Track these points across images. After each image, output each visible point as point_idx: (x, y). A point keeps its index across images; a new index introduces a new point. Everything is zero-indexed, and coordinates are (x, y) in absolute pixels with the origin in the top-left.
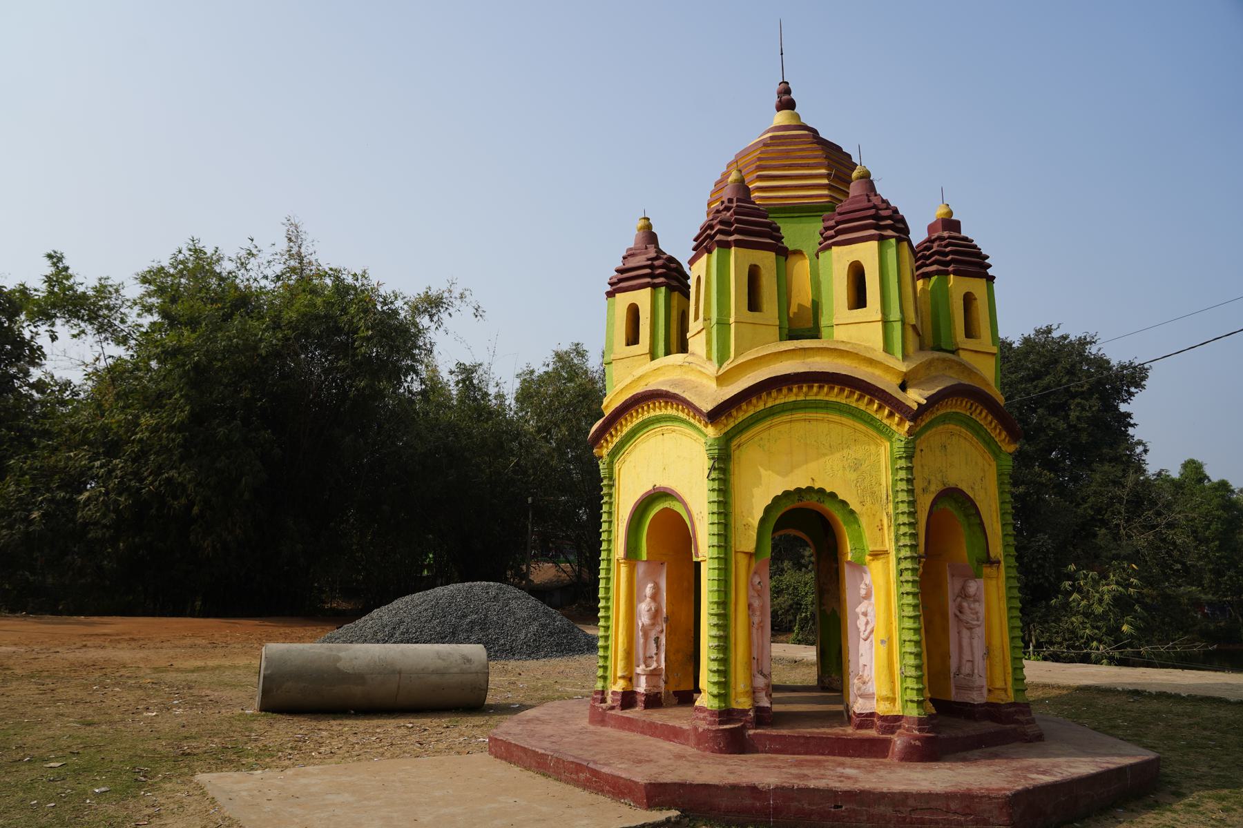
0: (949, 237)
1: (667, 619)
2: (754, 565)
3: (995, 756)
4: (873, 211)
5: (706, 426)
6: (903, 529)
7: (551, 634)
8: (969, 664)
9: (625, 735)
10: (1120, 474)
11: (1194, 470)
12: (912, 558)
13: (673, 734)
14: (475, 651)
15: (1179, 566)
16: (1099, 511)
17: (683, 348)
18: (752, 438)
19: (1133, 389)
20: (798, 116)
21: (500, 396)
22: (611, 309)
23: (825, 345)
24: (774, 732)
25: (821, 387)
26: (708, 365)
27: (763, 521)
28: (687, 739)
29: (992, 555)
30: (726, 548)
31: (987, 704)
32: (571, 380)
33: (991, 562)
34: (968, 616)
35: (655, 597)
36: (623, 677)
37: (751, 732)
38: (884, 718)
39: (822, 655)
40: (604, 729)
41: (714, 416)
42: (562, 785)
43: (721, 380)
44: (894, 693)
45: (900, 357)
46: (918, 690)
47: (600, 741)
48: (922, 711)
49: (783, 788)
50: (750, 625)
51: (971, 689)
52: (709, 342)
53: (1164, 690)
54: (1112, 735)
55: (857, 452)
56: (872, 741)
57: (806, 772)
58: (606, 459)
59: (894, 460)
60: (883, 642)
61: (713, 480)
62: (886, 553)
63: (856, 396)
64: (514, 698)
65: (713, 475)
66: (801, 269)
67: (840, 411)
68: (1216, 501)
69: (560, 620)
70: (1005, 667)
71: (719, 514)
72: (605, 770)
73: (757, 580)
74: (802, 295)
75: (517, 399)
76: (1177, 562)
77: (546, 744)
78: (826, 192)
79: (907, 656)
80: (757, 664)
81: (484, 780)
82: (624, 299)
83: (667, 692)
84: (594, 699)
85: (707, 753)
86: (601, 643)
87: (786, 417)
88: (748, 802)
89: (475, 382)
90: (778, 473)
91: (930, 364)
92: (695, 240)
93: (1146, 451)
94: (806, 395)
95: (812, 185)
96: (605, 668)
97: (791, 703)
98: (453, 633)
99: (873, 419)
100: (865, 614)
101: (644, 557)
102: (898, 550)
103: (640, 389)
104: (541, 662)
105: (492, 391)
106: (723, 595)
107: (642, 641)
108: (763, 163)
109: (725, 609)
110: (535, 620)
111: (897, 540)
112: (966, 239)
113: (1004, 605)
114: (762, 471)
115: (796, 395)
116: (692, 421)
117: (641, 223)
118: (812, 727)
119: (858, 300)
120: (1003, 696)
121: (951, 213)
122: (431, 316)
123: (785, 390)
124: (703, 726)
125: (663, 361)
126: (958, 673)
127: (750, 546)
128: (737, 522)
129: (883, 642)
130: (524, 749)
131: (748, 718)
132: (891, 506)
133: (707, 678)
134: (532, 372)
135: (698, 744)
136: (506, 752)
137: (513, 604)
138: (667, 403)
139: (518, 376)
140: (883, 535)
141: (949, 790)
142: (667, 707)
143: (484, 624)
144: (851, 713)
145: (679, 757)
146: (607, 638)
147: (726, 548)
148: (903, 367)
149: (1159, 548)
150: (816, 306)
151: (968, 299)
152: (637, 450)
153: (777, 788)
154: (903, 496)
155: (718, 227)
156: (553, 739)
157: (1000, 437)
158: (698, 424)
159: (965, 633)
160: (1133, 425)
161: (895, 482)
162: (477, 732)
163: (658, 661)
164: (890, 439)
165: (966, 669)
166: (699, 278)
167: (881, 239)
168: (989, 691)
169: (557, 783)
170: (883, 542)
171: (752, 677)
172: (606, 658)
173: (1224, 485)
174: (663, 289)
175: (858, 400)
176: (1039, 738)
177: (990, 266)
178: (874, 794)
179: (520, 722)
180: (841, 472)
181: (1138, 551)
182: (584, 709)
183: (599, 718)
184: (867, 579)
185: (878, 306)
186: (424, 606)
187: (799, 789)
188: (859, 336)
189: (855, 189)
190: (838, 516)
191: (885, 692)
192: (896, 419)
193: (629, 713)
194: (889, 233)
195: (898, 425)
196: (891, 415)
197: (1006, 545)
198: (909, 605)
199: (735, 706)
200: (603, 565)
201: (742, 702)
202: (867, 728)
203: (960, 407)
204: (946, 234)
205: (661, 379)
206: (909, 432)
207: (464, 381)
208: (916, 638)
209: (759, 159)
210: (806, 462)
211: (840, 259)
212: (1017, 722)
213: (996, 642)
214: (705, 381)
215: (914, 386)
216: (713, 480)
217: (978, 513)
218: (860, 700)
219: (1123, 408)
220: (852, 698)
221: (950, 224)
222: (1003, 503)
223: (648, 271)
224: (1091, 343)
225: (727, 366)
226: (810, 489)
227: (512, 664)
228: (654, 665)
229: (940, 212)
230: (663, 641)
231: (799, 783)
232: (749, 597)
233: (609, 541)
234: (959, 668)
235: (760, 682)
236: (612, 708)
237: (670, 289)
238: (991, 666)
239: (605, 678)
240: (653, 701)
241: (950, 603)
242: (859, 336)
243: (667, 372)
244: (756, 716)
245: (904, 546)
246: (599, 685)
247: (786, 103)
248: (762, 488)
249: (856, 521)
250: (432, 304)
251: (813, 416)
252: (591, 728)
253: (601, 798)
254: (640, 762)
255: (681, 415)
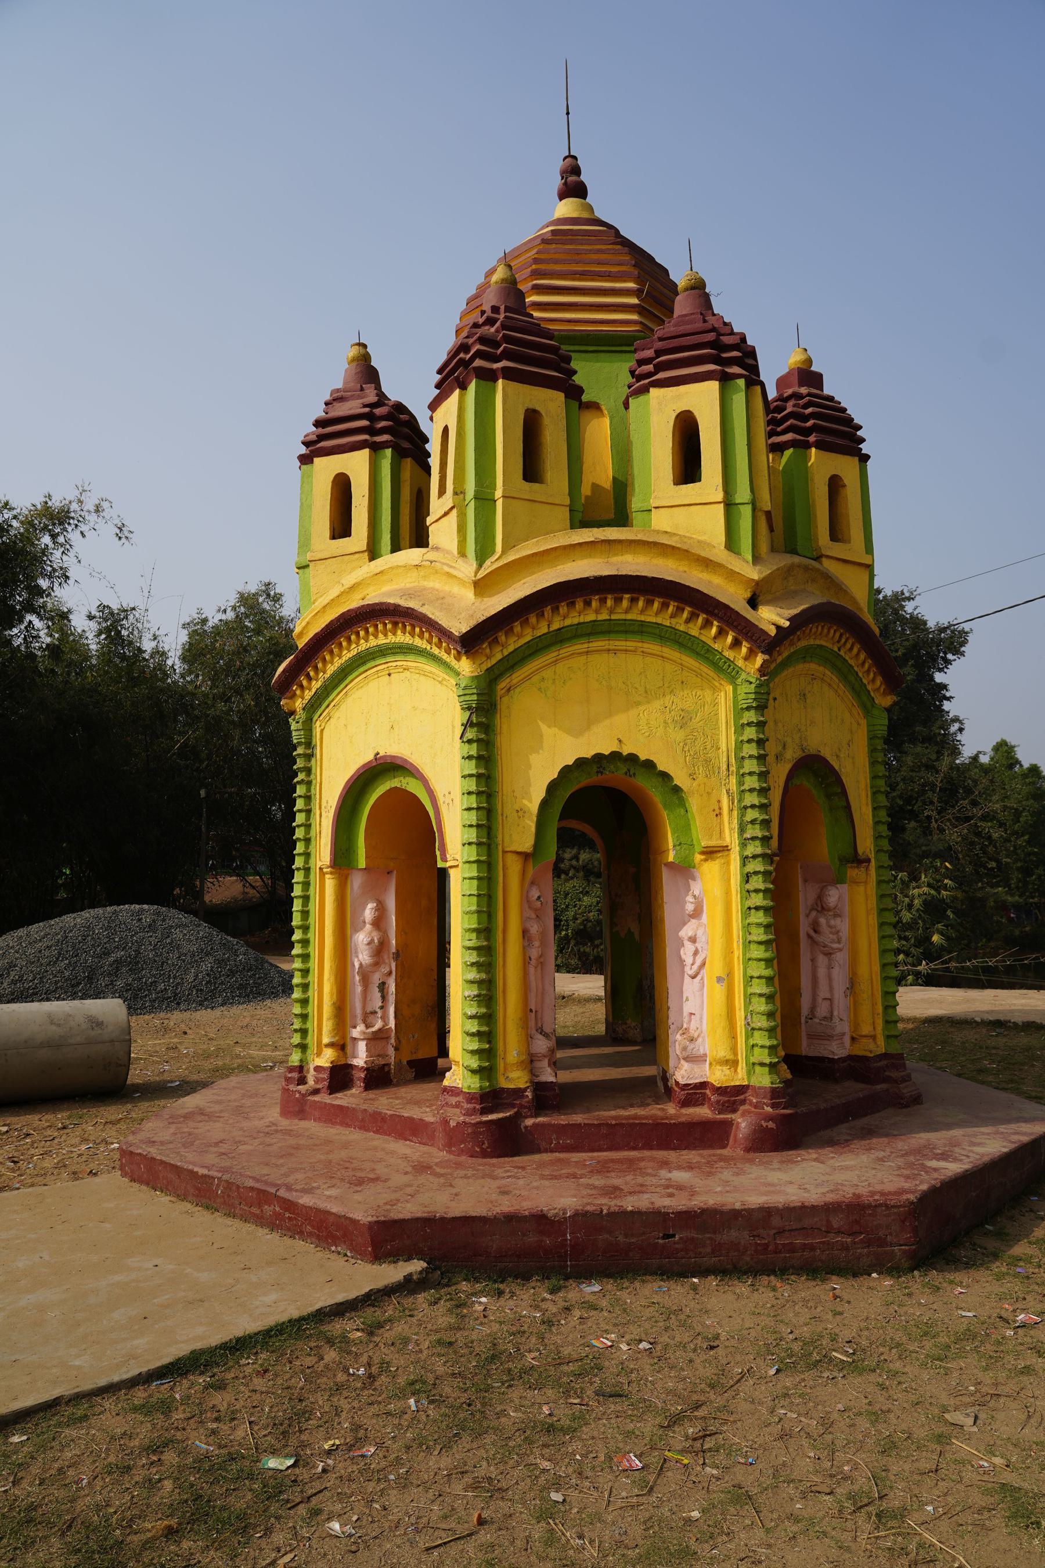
0: (809, 395)
1: (397, 956)
2: (530, 872)
3: (868, 1133)
4: (711, 336)
5: (458, 658)
6: (751, 815)
7: (232, 973)
8: (827, 1003)
9: (335, 1132)
10: (934, 757)
11: (1004, 750)
12: (763, 856)
13: (410, 1129)
14: (110, 1008)
15: (994, 864)
16: (909, 800)
17: (420, 539)
18: (529, 677)
19: (950, 656)
20: (590, 209)
21: (160, 654)
22: (306, 482)
23: (640, 537)
24: (562, 1120)
25: (634, 601)
26: (460, 563)
27: (544, 804)
28: (432, 1137)
29: (860, 851)
30: (489, 846)
31: (850, 1057)
32: (258, 632)
33: (858, 860)
34: (826, 937)
35: (378, 923)
36: (331, 1045)
37: (529, 1122)
38: (722, 1091)
39: (614, 992)
40: (304, 1124)
41: (471, 642)
42: (237, 1223)
43: (481, 586)
44: (735, 1054)
45: (750, 558)
46: (771, 1048)
47: (297, 1148)
48: (775, 1077)
49: (585, 1214)
50: (526, 961)
51: (829, 1037)
52: (461, 529)
53: (1031, 1019)
54: (983, 1083)
55: (685, 699)
56: (705, 1125)
57: (617, 1182)
58: (300, 715)
59: (739, 712)
60: (719, 979)
61: (469, 741)
62: (726, 849)
63: (685, 615)
64: (173, 1071)
65: (470, 734)
66: (599, 432)
67: (661, 637)
68: (1026, 789)
69: (244, 954)
70: (874, 1005)
71: (479, 794)
72: (306, 1200)
73: (535, 893)
74: (600, 469)
75: (184, 659)
76: (991, 859)
77: (211, 1158)
78: (635, 317)
79: (755, 1000)
80: (533, 1020)
81: (107, 1225)
82: (327, 467)
83: (398, 1063)
84: (288, 1080)
85: (463, 1158)
86: (296, 980)
87: (580, 646)
88: (532, 1239)
89: (124, 633)
90: (569, 731)
91: (787, 572)
92: (439, 372)
93: (961, 730)
94: (611, 612)
95: (617, 307)
96: (304, 1032)
97: (578, 1067)
98: (90, 978)
99: (710, 650)
100: (693, 940)
101: (362, 863)
102: (743, 845)
103: (354, 602)
104: (217, 1012)
105: (148, 646)
106: (485, 916)
107: (359, 989)
108: (542, 267)
109: (488, 939)
110: (208, 954)
111: (742, 830)
112: (831, 399)
113: (874, 921)
114: (544, 727)
115: (597, 612)
116: (436, 651)
117: (353, 352)
118: (616, 1108)
119: (688, 468)
120: (872, 1046)
121: (809, 361)
122: (54, 537)
123: (579, 604)
124: (456, 1117)
125: (388, 560)
126: (812, 1015)
127: (527, 843)
128: (506, 806)
129: (719, 979)
130: (175, 1168)
131: (524, 1101)
132: (733, 780)
133: (460, 1044)
134: (205, 621)
135: (449, 1145)
136: (147, 1171)
137: (177, 934)
138: (395, 624)
139: (184, 626)
140: (721, 823)
141: (831, 1198)
142: (398, 1085)
143: (134, 964)
144: (671, 1083)
145: (422, 1168)
146: (305, 972)
147: (489, 846)
148: (754, 574)
149: (972, 843)
150: (622, 488)
151: (835, 484)
152: (349, 700)
153: (576, 1214)
154: (751, 765)
155: (478, 347)
156: (223, 1148)
157: (874, 683)
158: (444, 656)
159: (822, 961)
160: (948, 699)
161: (739, 744)
162: (111, 1132)
163: (384, 1018)
164: (733, 679)
165: (822, 1010)
166: (446, 430)
167: (725, 379)
168: (853, 1039)
169: (229, 1221)
170: (721, 832)
171: (529, 1038)
172: (305, 1002)
173: (1034, 770)
174: (388, 452)
175: (688, 621)
176: (917, 1100)
177: (863, 440)
178: (721, 1213)
179: (173, 1119)
180: (661, 730)
181: (950, 848)
182: (270, 1089)
183: (296, 1107)
184: (696, 888)
185: (719, 480)
186: (46, 942)
187: (610, 1214)
188: (691, 523)
189: (682, 306)
190: (656, 795)
191: (723, 1052)
192: (744, 650)
193: (342, 1099)
194: (736, 370)
195: (746, 659)
196: (736, 644)
197: (878, 837)
198: (759, 925)
199: (504, 1084)
200: (298, 877)
201: (515, 1078)
202: (695, 1105)
203: (825, 638)
204: (804, 390)
205: (386, 588)
206: (762, 670)
207: (108, 630)
208: (768, 972)
209: (536, 261)
210: (610, 714)
211: (662, 406)
212: (887, 1080)
213: (863, 971)
214: (456, 589)
215: (768, 603)
216: (469, 741)
217: (844, 792)
218: (685, 1065)
219: (939, 677)
220: (672, 1062)
221: (808, 376)
222: (874, 777)
223: (364, 423)
224: (909, 599)
225: (489, 566)
226: (615, 756)
227: (176, 1017)
228: (379, 1025)
229: (795, 359)
230: (392, 988)
231: (608, 1204)
232: (524, 920)
233: (307, 841)
234: (813, 1009)
235: (542, 1045)
236: (316, 1092)
237: (400, 454)
238: (856, 1005)
239: (303, 1047)
240: (378, 1078)
241: (802, 918)
242: (691, 523)
243: (394, 576)
244: (537, 1097)
245: (753, 838)
246: (295, 1058)
247: (573, 187)
248: (544, 754)
249: (682, 802)
250: (56, 518)
251: (621, 644)
252: (285, 1123)
253: (299, 1244)
254: (360, 1182)
255: (418, 642)
